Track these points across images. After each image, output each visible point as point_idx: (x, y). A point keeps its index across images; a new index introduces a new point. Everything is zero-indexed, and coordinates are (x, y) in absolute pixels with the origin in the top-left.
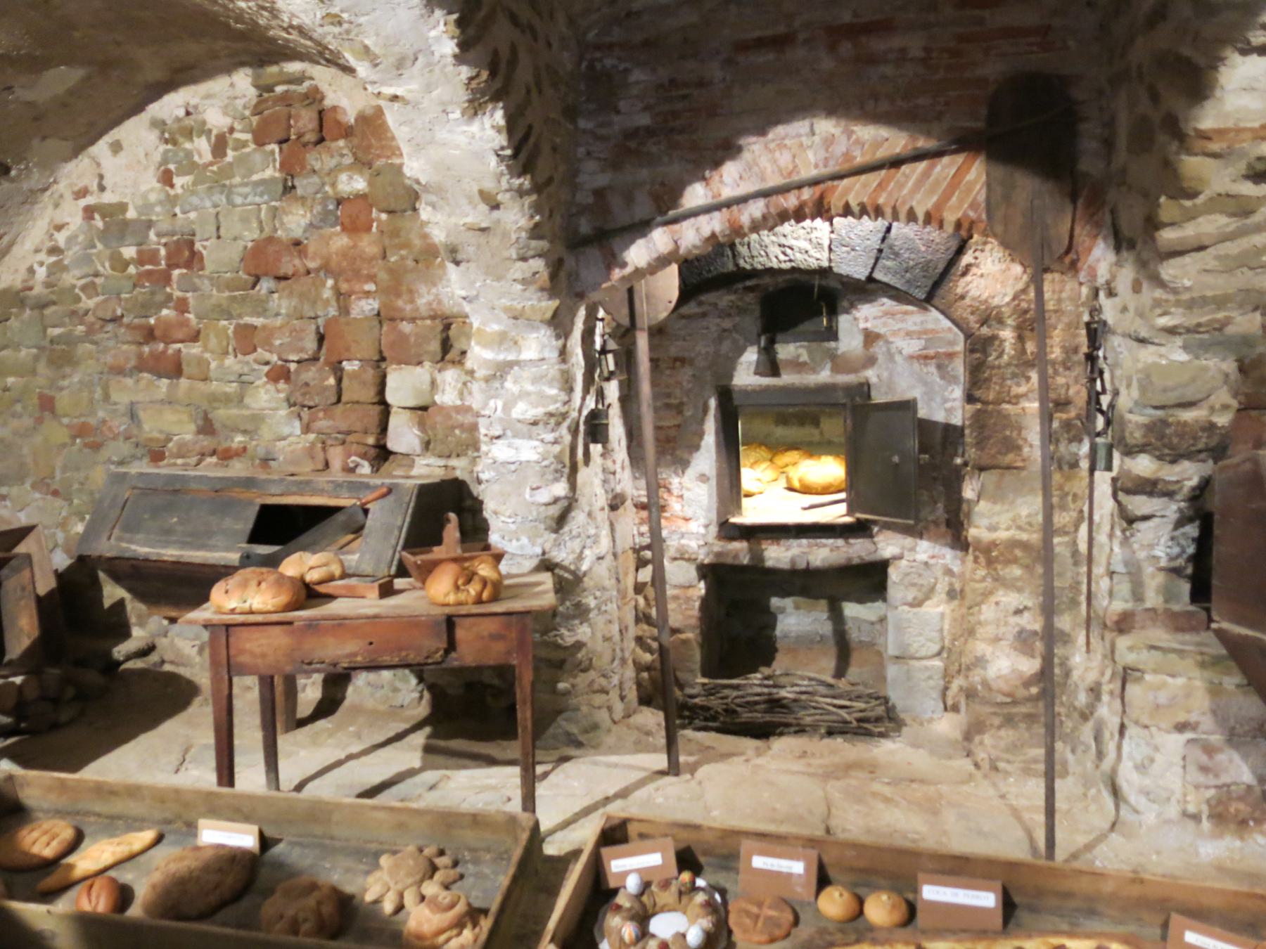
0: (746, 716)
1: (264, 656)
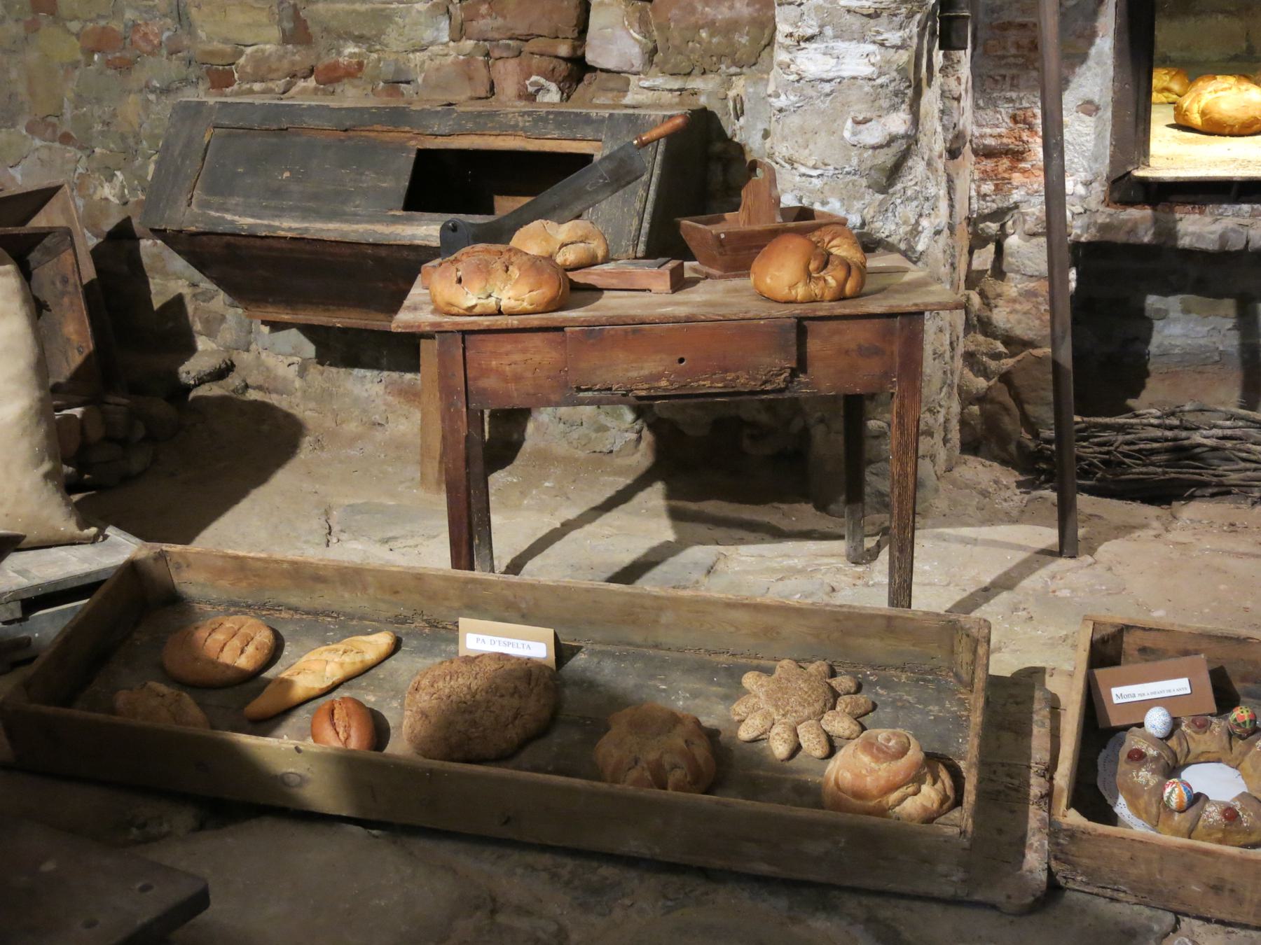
0: (1138, 471)
1: (518, 378)
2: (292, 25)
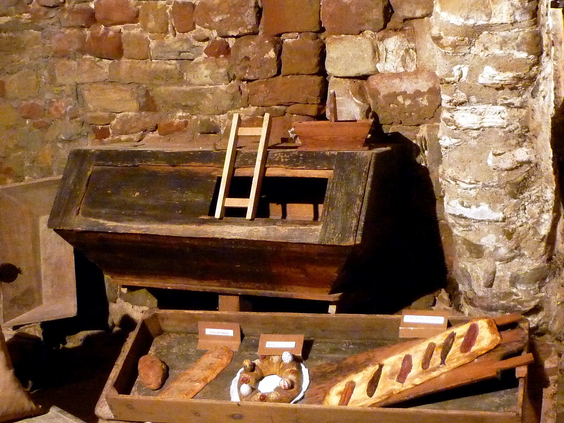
2: (144, 100)
